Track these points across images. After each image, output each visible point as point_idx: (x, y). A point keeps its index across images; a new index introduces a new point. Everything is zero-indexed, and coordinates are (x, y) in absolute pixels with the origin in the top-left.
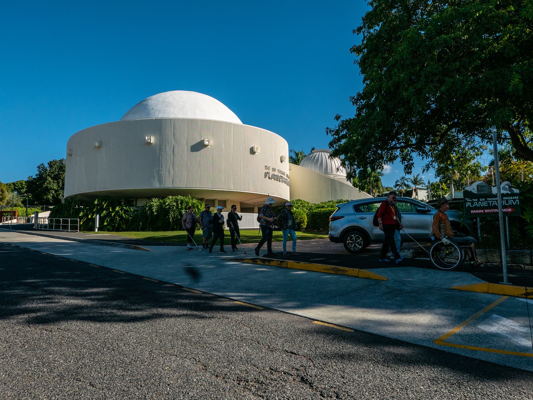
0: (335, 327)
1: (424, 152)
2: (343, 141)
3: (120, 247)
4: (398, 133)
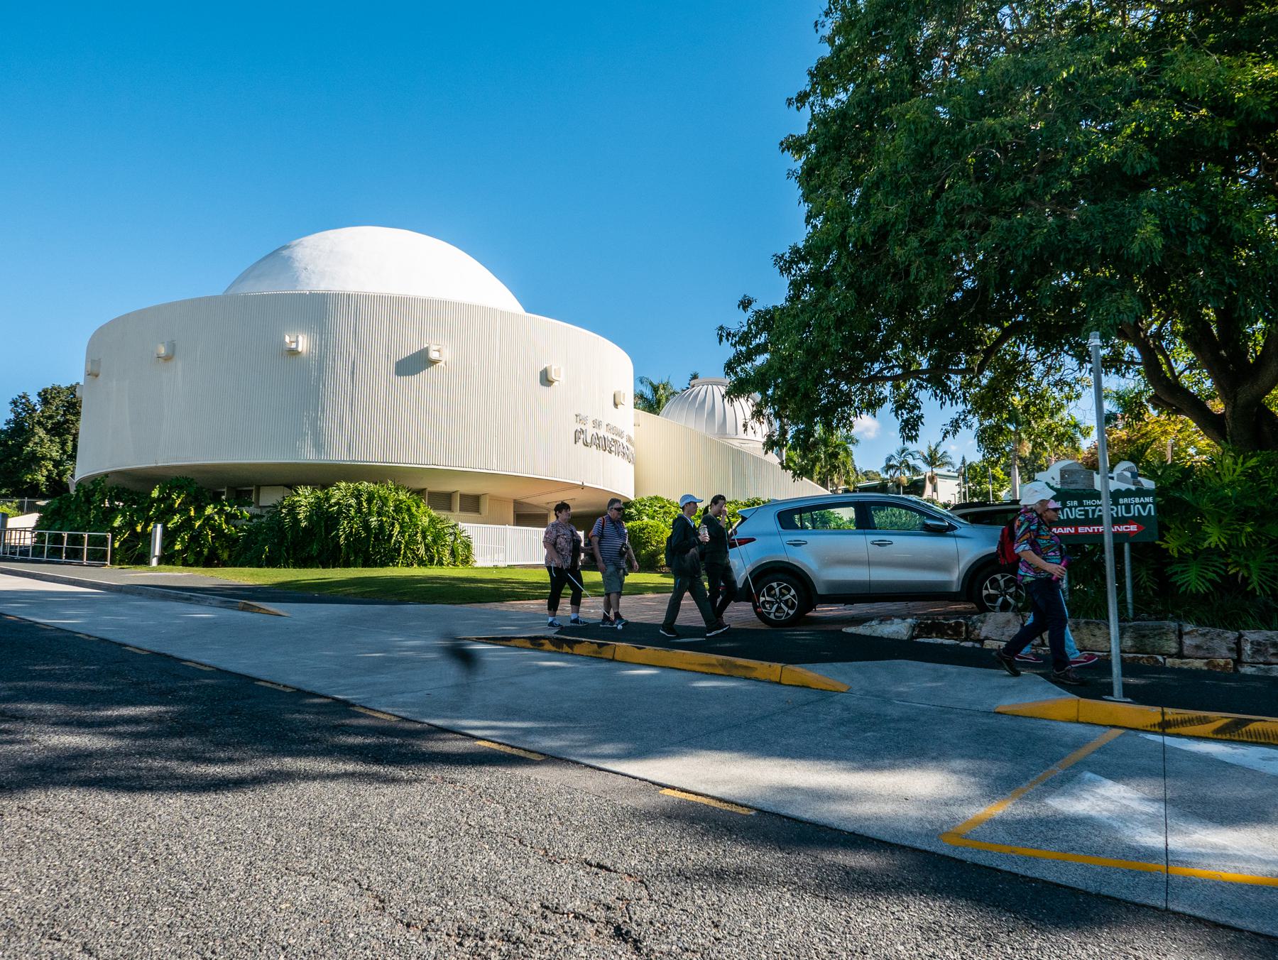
0: (713, 803)
1: (946, 390)
2: (760, 360)
3: (211, 605)
4: (888, 344)
